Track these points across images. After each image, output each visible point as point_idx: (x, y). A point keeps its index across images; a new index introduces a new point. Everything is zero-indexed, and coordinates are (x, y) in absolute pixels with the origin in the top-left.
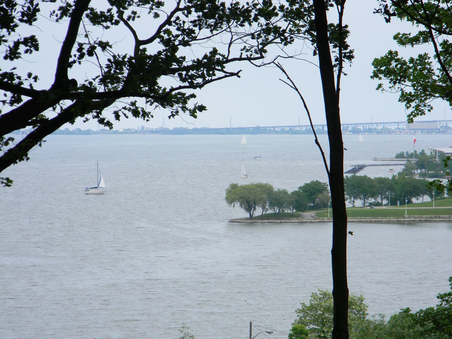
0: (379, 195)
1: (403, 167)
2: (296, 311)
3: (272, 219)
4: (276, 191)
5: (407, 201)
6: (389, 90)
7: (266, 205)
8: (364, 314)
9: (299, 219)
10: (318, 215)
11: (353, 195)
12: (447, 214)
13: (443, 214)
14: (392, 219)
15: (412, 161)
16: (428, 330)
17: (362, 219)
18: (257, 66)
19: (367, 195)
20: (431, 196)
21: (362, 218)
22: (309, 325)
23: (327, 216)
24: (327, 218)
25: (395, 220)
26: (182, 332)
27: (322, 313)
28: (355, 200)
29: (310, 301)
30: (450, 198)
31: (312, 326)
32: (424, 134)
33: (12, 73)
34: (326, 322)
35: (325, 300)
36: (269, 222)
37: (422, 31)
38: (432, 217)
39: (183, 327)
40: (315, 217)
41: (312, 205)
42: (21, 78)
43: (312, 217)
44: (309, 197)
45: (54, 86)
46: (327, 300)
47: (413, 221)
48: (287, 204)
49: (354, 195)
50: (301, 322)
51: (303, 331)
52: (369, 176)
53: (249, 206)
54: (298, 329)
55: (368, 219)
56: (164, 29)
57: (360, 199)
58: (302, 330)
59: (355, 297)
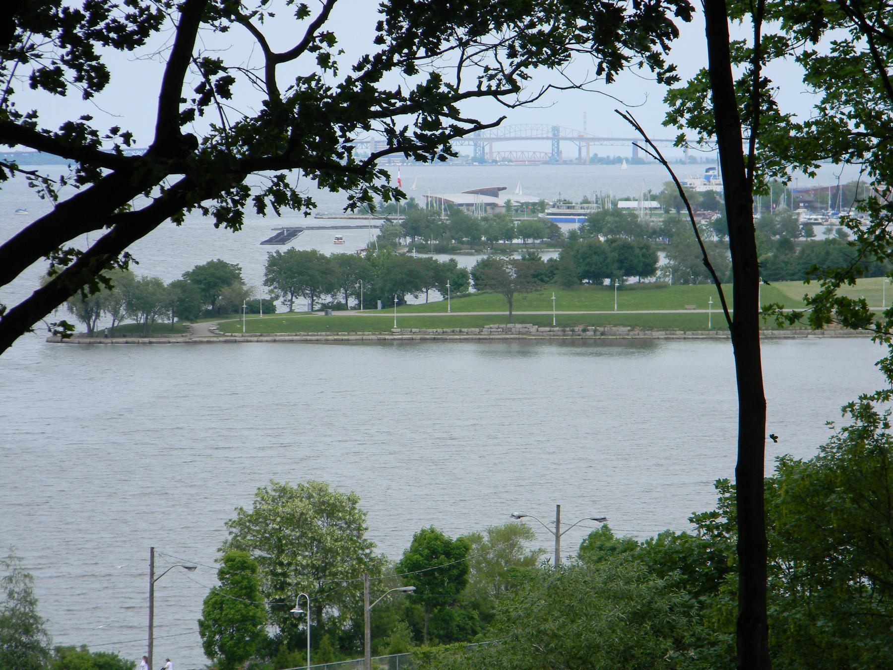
0: (342, 289)
1: (377, 232)
2: (226, 523)
3: (132, 336)
4: (139, 282)
5: (396, 300)
6: (698, 146)
7: (119, 309)
8: (359, 529)
9: (186, 336)
10: (222, 328)
11: (291, 288)
12: (474, 327)
13: (468, 327)
14: (368, 335)
15: (394, 219)
16: (672, 583)
17: (308, 335)
18: (509, 106)
19: (318, 288)
20: (443, 291)
21: (310, 333)
22: (252, 550)
23: (240, 330)
24: (240, 335)
25: (374, 337)
26: (8, 566)
27: (277, 527)
28: (294, 298)
29: (255, 503)
30: (480, 294)
31: (257, 553)
32: (407, 165)
33: (82, 124)
34: (286, 545)
35: (283, 503)
36: (127, 343)
37: (769, 35)
38: (446, 332)
39: (10, 557)
40: (217, 332)
41: (210, 308)
42: (98, 133)
43: (211, 331)
44: (203, 294)
45: (152, 148)
46: (287, 502)
47: (409, 339)
48: (162, 307)
49: (292, 289)
50: (236, 544)
51: (246, 563)
52: (321, 253)
53: (86, 311)
54: (237, 560)
55: (321, 335)
56: (316, 34)
57: (305, 295)
58: (245, 562)
59: (341, 495)
